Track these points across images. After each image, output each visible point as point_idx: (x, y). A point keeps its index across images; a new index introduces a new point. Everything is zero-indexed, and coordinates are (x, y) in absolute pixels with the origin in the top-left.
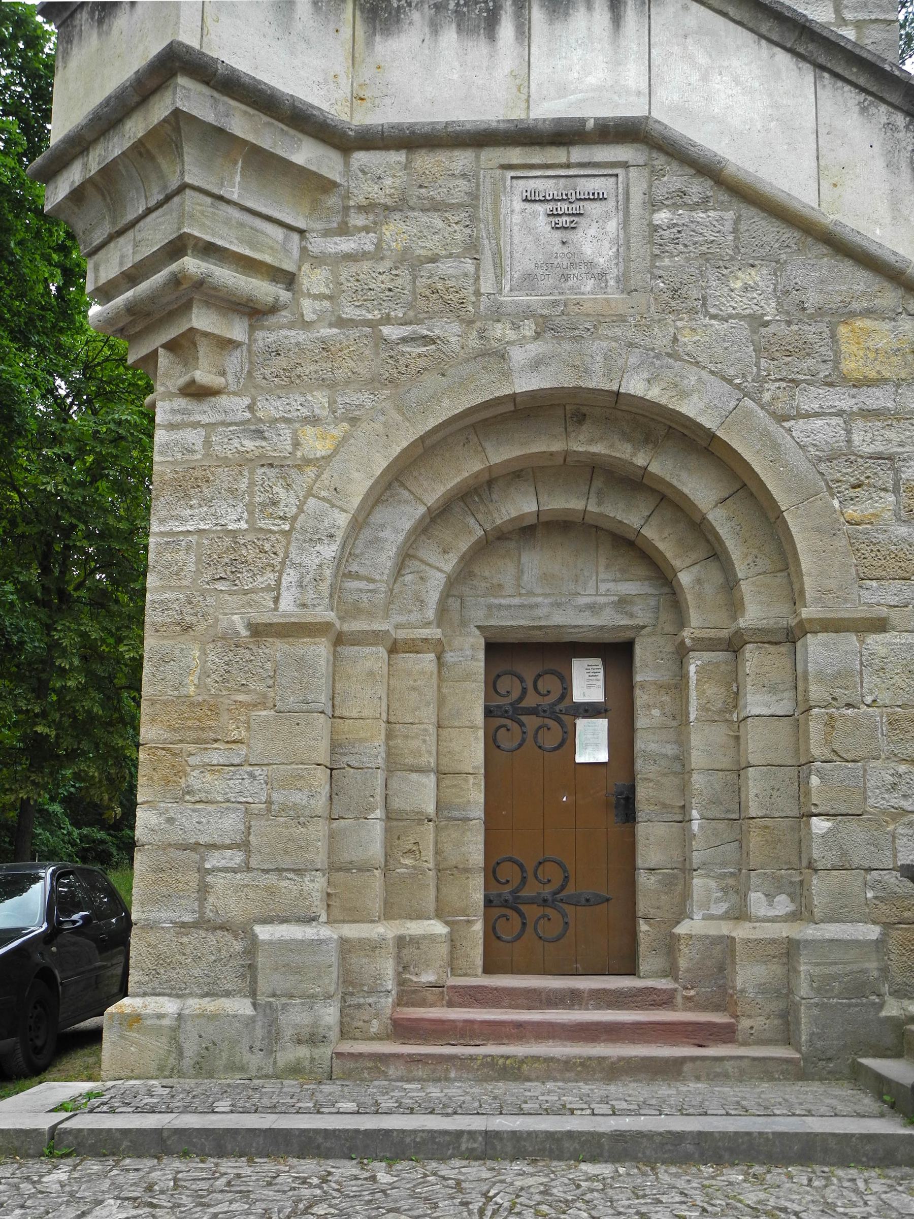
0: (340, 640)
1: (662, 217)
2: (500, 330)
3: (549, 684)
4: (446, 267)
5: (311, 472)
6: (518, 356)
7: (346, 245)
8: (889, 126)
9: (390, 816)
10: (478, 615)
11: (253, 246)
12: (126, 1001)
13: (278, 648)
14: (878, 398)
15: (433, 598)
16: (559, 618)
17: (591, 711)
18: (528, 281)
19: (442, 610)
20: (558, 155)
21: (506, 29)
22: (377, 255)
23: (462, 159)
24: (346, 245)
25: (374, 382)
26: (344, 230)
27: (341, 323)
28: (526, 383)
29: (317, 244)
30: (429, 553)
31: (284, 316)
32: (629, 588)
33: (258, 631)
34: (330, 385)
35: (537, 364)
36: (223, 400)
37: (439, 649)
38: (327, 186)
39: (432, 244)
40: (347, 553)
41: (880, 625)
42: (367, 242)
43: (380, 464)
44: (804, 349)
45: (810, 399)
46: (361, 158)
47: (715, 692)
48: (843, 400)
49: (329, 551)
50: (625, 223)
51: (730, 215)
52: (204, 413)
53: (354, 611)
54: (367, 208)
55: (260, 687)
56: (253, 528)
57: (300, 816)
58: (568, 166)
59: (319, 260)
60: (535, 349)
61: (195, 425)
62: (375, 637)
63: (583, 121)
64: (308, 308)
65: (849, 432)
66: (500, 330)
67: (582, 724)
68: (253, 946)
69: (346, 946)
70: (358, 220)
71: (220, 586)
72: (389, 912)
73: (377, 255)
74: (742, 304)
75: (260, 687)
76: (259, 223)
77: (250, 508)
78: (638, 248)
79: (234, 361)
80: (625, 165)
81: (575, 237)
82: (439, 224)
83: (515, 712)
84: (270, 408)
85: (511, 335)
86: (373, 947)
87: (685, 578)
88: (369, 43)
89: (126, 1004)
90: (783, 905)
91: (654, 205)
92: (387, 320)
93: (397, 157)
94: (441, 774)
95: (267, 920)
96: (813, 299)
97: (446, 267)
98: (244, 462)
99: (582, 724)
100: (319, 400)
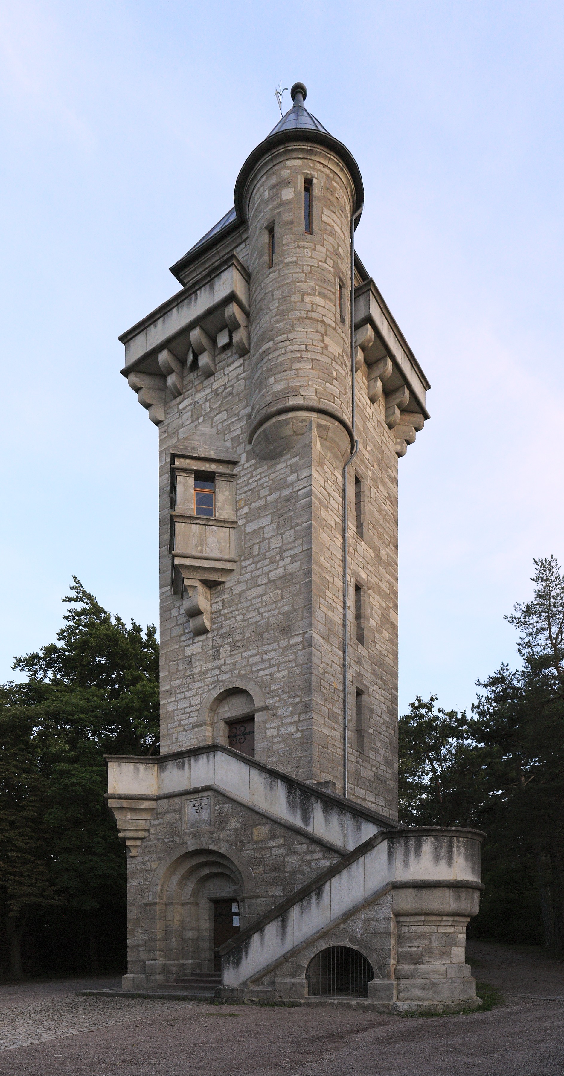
1: (217, 807)
4: (176, 825)
5: (153, 871)
6: (189, 843)
8: (265, 778)
20: (196, 795)
23: (177, 800)
24: (157, 822)
26: (157, 819)
27: (158, 839)
28: (191, 849)
31: (147, 839)
33: (146, 905)
34: (156, 853)
36: (138, 858)
39: (173, 820)
51: (231, 805)
54: (161, 813)
55: (146, 916)
56: (144, 884)
60: (192, 841)
63: (198, 788)
64: (152, 837)
66: (186, 838)
67: (234, 917)
70: (159, 816)
75: (146, 916)
76: (137, 821)
77: (144, 880)
80: (210, 796)
81: (201, 814)
84: (147, 859)
85: (188, 838)
88: (160, 774)
93: (166, 801)
95: (149, 960)
97: (176, 825)
98: (142, 870)
99: (234, 917)
100: (154, 856)
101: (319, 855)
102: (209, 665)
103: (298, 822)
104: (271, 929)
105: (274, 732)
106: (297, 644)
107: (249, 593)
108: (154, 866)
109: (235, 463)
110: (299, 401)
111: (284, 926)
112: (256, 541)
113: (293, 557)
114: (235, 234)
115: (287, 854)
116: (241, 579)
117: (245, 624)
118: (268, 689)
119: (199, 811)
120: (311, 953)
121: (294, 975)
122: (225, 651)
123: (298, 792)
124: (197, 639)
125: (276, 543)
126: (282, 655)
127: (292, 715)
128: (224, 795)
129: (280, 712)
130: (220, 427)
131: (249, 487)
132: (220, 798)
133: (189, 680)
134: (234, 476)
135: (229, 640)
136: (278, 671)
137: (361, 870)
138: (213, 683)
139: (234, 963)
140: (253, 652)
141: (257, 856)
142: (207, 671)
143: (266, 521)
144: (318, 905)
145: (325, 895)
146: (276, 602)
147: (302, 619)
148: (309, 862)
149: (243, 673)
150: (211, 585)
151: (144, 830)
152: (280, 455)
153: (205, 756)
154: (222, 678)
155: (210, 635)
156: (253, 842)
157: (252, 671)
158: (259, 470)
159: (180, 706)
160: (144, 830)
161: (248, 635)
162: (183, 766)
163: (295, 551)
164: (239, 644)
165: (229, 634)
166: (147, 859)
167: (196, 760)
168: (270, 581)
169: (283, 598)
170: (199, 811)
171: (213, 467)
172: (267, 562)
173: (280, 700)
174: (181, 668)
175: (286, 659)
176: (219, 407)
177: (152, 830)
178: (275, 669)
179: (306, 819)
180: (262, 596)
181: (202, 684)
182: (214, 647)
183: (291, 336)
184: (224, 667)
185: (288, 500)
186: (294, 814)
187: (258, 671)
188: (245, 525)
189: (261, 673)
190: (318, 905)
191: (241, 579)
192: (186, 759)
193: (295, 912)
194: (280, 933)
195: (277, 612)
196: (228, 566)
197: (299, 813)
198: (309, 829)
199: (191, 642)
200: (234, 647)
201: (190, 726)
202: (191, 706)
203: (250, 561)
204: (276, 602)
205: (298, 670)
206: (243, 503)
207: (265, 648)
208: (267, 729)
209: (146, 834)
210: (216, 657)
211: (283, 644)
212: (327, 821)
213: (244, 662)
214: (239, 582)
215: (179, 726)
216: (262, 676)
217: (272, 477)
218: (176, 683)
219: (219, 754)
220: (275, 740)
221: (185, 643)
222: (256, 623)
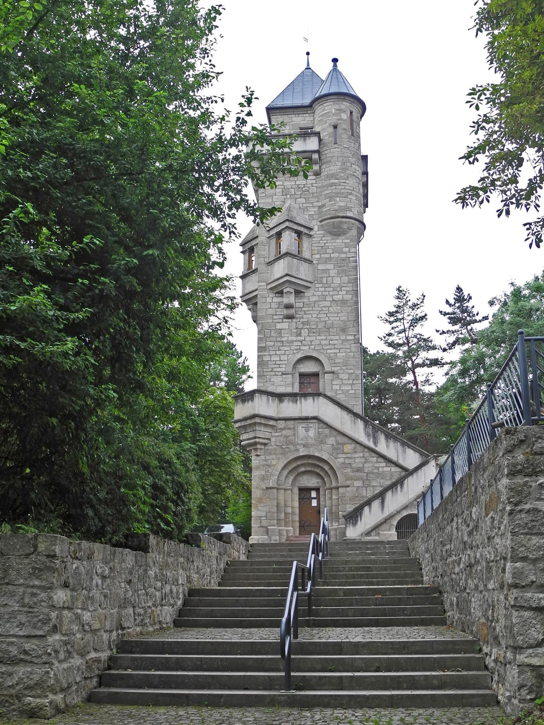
0: (278, 489)
2: (298, 447)
3: (308, 494)
4: (291, 438)
6: (301, 450)
7: (277, 434)
9: (285, 513)
10: (297, 485)
13: (270, 490)
14: (349, 455)
15: (290, 483)
16: (309, 485)
17: (314, 498)
18: (302, 439)
19: (292, 484)
21: (298, 402)
22: (281, 436)
23: (292, 422)
24: (277, 434)
25: (282, 454)
28: (302, 454)
29: (273, 434)
30: (290, 476)
32: (319, 480)
33: (267, 488)
34: (275, 454)
35: (303, 451)
37: (292, 490)
38: (274, 426)
40: (279, 477)
41: (348, 486)
42: (280, 434)
43: (283, 465)
44: (339, 449)
45: (340, 456)
46: (279, 422)
47: (329, 495)
48: (344, 456)
49: (276, 477)
52: (259, 458)
53: (279, 485)
57: (273, 513)
59: (274, 436)
60: (303, 449)
62: (282, 489)
64: (272, 443)
66: (298, 447)
68: (268, 529)
69: (280, 530)
72: (285, 526)
73: (281, 436)
74: (331, 442)
78: (317, 434)
79: (262, 451)
83: (303, 498)
84: (267, 457)
86: (283, 530)
90: (337, 524)
91: (319, 428)
94: (292, 508)
96: (340, 442)
97: (291, 438)
98: (264, 465)
100: (274, 456)
101: (384, 464)
102: (294, 338)
103: (371, 444)
104: (376, 504)
105: (337, 387)
106: (351, 340)
107: (320, 303)
108: (274, 462)
109: (311, 229)
110: (349, 214)
111: (383, 502)
112: (325, 275)
113: (347, 291)
114: (306, 109)
115: (365, 462)
116: (315, 293)
117: (318, 320)
118: (333, 361)
119: (307, 430)
120: (398, 518)
121: (389, 530)
122: (305, 332)
123: (371, 427)
124: (285, 320)
125: (337, 280)
126: (342, 344)
127: (349, 379)
128: (326, 424)
129: (341, 376)
130: (301, 205)
131: (320, 245)
132: (322, 425)
133: (279, 344)
134: (311, 236)
135: (308, 327)
136: (340, 352)
137: (423, 474)
138: (296, 350)
139: (353, 524)
140: (324, 338)
141: (347, 461)
142: (292, 342)
143: (331, 267)
144: (401, 491)
145: (405, 486)
146: (338, 313)
147: (353, 326)
148: (378, 468)
149: (317, 348)
150: (298, 293)
151: (267, 439)
152: (339, 235)
153: (311, 398)
154: (302, 348)
155: (294, 320)
156: (344, 453)
157: (323, 349)
158: (326, 238)
159: (272, 359)
160: (267, 439)
161: (319, 327)
162: (296, 401)
163: (348, 289)
164: (314, 330)
165: (308, 323)
166: (267, 457)
167: (306, 400)
168: (333, 300)
169: (342, 312)
170: (307, 430)
171: (302, 229)
172: (332, 289)
173: (341, 369)
174: (272, 335)
175: (344, 347)
176: (301, 194)
177: (273, 439)
178: (337, 351)
179: (375, 443)
180: (329, 307)
181: (289, 349)
182: (297, 328)
183: (347, 182)
184: (304, 342)
185: (343, 260)
186: (369, 440)
187: (327, 349)
188: (318, 264)
189: (329, 351)
190: (401, 491)
191: (315, 293)
192: (298, 398)
193: (389, 494)
194: (380, 506)
195: (338, 318)
196: (308, 285)
197: (372, 439)
198: (378, 449)
199: (281, 321)
200: (310, 330)
201: (280, 373)
202: (280, 360)
203: (321, 285)
204: (338, 313)
205: (352, 354)
206: (316, 252)
207: (332, 337)
208: (332, 384)
209: (268, 441)
210: (300, 335)
211: (343, 337)
212: (388, 446)
213: (318, 342)
214: (314, 295)
215: (271, 371)
216: (330, 353)
217: (334, 244)
218: (269, 344)
219: (321, 398)
220: (338, 392)
221: (277, 321)
222: (326, 321)
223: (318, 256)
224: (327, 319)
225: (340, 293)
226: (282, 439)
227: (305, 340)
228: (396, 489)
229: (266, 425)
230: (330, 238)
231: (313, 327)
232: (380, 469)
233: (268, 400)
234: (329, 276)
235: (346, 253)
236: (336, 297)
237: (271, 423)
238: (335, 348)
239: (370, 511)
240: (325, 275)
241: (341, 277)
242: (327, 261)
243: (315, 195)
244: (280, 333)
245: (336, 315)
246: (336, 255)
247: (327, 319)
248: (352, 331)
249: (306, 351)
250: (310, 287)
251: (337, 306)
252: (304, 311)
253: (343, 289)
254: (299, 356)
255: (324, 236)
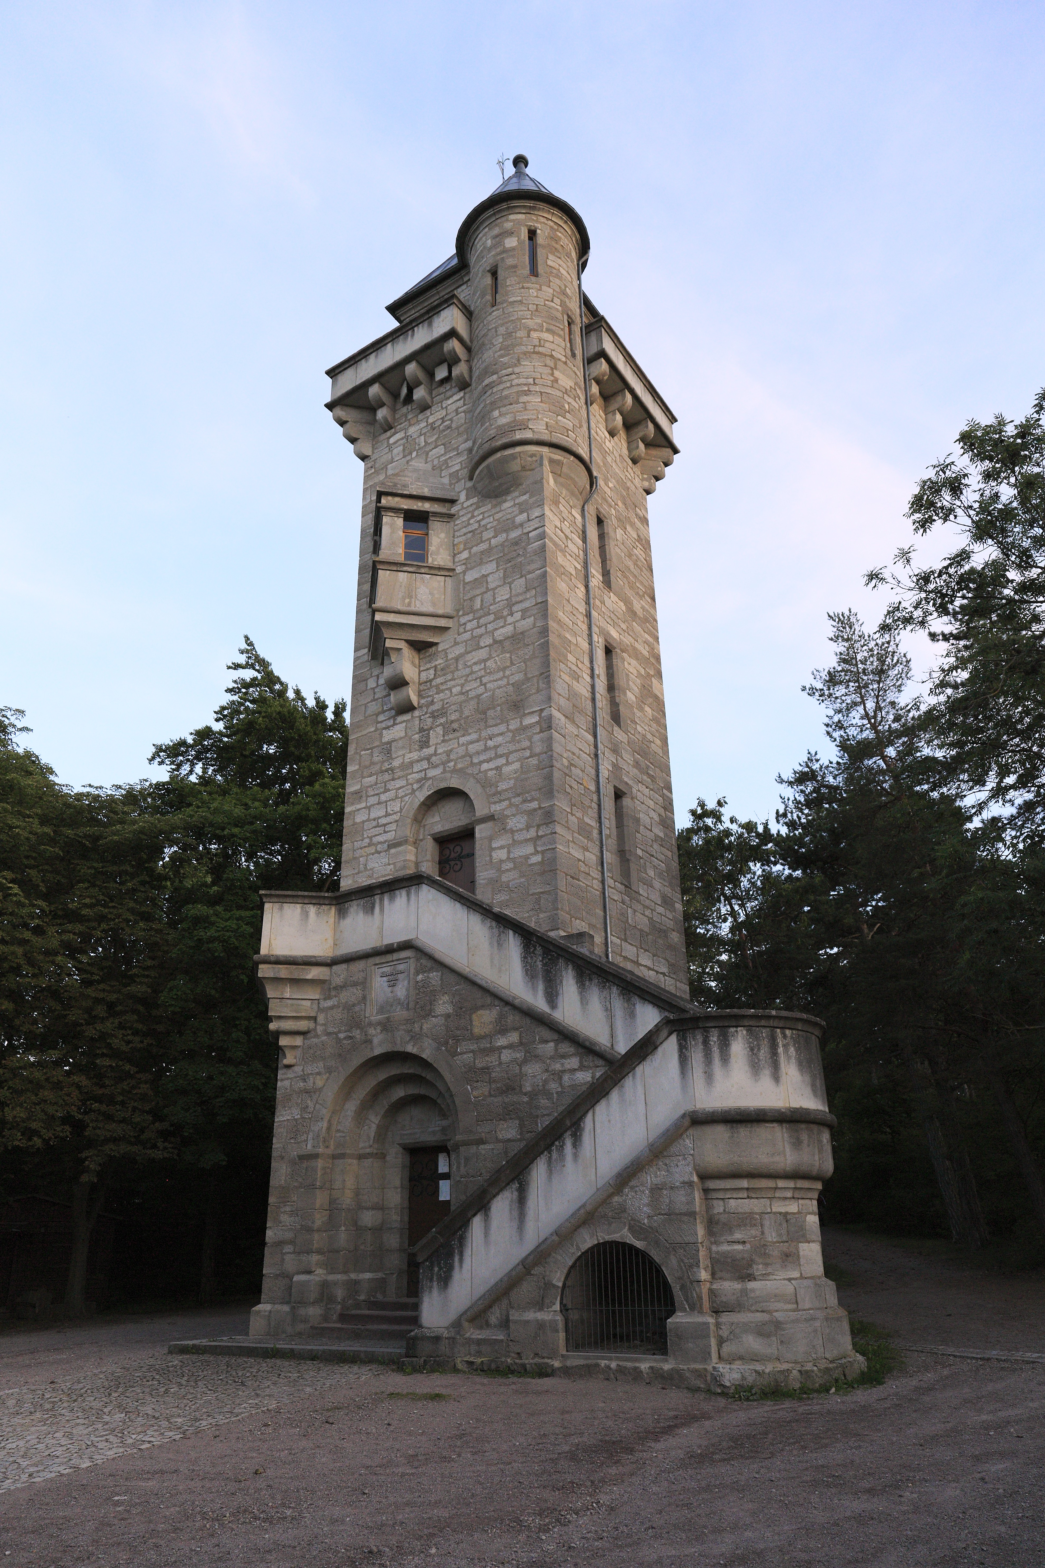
1: (420, 977)
6: (376, 1041)
8: (491, 927)
11: (296, 1012)
12: (260, 1306)
20: (389, 957)
33: (302, 1158)
50: (409, 982)
54: (335, 988)
58: (393, 961)
61: (287, 1079)
63: (393, 944)
64: (320, 1029)
65: (475, 1059)
66: (371, 1031)
70: (333, 993)
71: (292, 1141)
80: (409, 958)
82: (355, 991)
87: (428, 1077)
88: (339, 923)
89: (260, 1307)
92: (340, 1032)
93: (344, 966)
95: (299, 1273)
97: (357, 1009)
102: (415, 755)
103: (540, 1003)
105: (502, 854)
106: (531, 726)
107: (468, 657)
111: (522, 1200)
112: (478, 592)
113: (524, 611)
114: (457, 277)
115: (525, 1061)
117: (463, 698)
118: (493, 790)
120: (567, 1258)
122: (436, 736)
124: (400, 719)
125: (503, 594)
127: (528, 828)
128: (430, 957)
129: (511, 823)
131: (470, 529)
133: (387, 777)
134: (451, 516)
135: (442, 720)
136: (508, 763)
140: (474, 736)
141: (480, 1064)
143: (491, 567)
144: (576, 1156)
146: (504, 669)
148: (558, 1075)
151: (309, 1018)
152: (507, 492)
155: (416, 713)
157: (472, 764)
158: (482, 510)
160: (309, 1018)
161: (467, 713)
162: (373, 908)
163: (527, 604)
164: (455, 726)
165: (443, 712)
167: (392, 899)
168: (495, 642)
169: (512, 664)
171: (427, 506)
172: (492, 617)
174: (376, 759)
175: (518, 746)
176: (436, 441)
177: (321, 1018)
178: (503, 761)
180: (485, 661)
181: (404, 783)
184: (434, 759)
185: (516, 544)
186: (534, 988)
187: (481, 763)
188: (464, 572)
189: (485, 766)
190: (576, 1156)
192: (377, 898)
193: (539, 1171)
195: (505, 681)
196: (442, 623)
197: (541, 987)
199: (391, 722)
203: (471, 617)
204: (504, 669)
207: (490, 731)
211: (514, 725)
212: (584, 1001)
213: (461, 751)
214: (456, 644)
215: (370, 845)
216: (486, 771)
217: (497, 516)
219: (425, 888)
220: (505, 867)
221: (383, 725)
223: (465, 555)
224: (481, 690)
225: (510, 619)
226: (338, 1014)
227: (435, 754)
228: (562, 1148)
229: (296, 982)
230: (489, 506)
231: (453, 717)
232: (566, 1077)
233: (306, 915)
234: (488, 590)
235: (521, 525)
236: (500, 634)
237: (314, 973)
238: (497, 756)
239: (486, 1234)
240: (478, 592)
241: (510, 584)
242: (480, 560)
243: (462, 429)
244: (389, 752)
245: (501, 674)
246: (502, 538)
247: (481, 690)
248: (534, 703)
249: (439, 778)
250: (447, 629)
251: (503, 652)
252: (437, 686)
253: (515, 608)
254: (422, 795)
255: (478, 508)
